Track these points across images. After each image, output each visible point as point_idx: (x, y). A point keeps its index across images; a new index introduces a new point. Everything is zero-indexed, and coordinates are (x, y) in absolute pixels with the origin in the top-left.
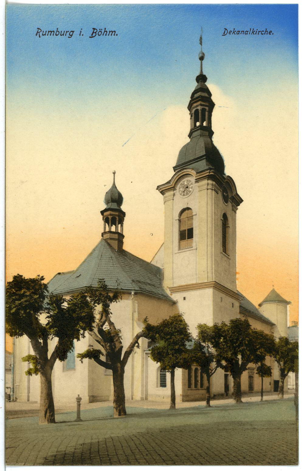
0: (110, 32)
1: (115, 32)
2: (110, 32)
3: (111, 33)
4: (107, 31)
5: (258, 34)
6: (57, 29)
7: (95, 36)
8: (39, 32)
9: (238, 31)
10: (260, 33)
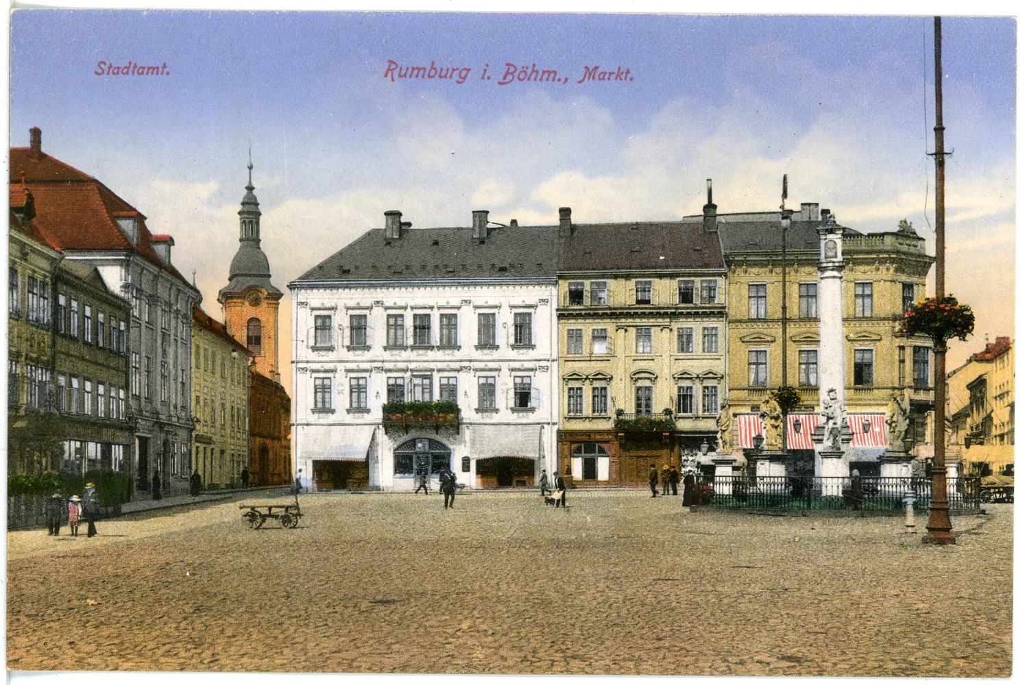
0: (544, 72)
1: (555, 72)
2: (544, 72)
3: (546, 75)
4: (537, 72)
5: (609, 79)
6: (433, 63)
7: (511, 81)
8: (392, 70)
9: (466, 69)
10: (613, 77)
